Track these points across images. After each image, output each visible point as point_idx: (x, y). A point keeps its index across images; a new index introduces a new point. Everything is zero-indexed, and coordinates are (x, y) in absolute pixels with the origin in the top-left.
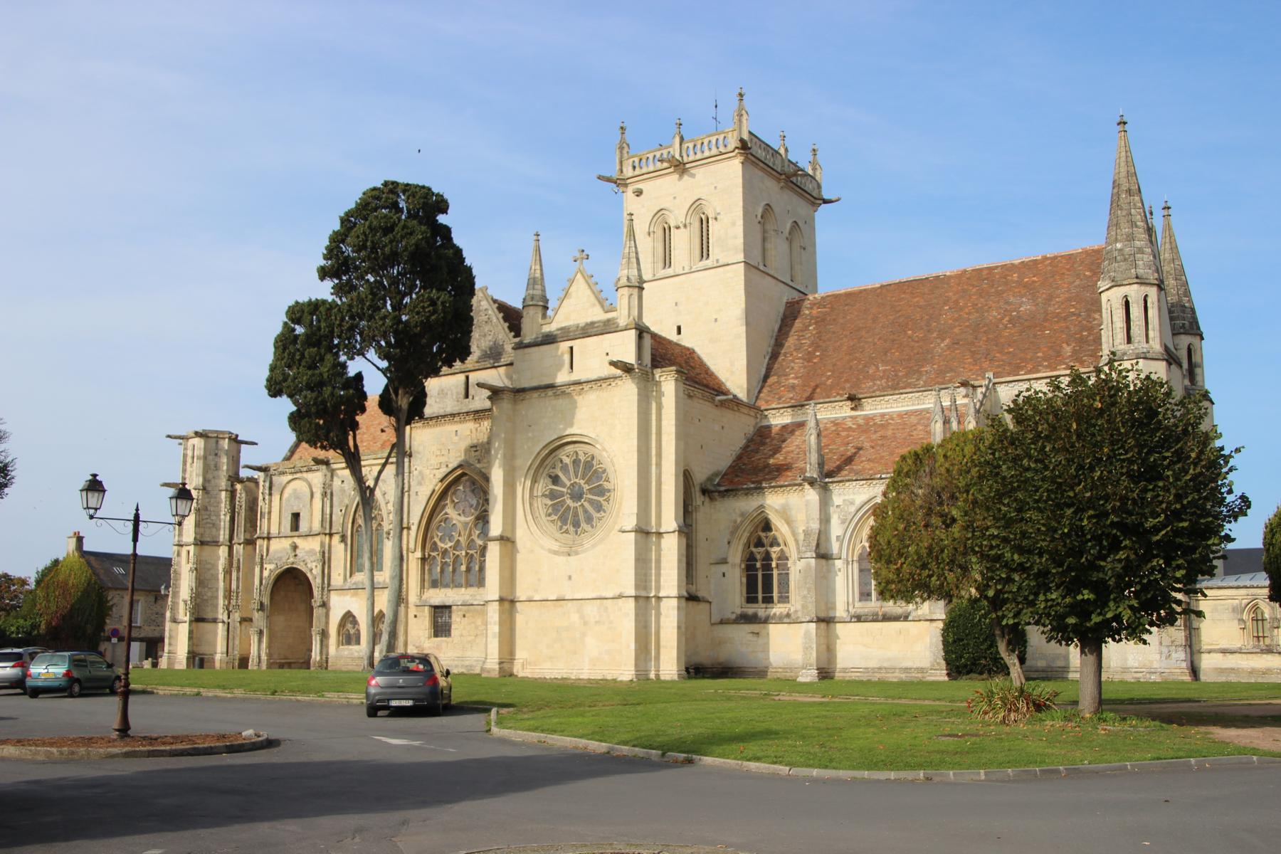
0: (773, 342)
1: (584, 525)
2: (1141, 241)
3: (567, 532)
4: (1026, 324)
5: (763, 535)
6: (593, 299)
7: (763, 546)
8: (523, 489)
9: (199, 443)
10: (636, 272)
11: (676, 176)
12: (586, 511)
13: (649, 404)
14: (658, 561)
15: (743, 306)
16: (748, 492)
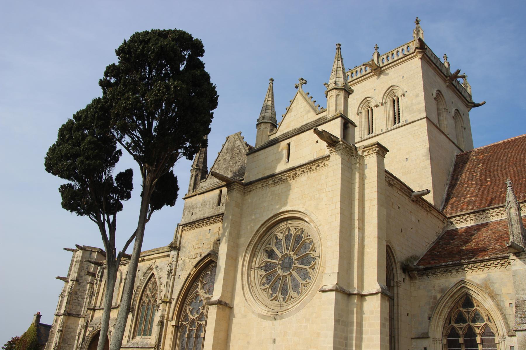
0: (450, 178)
1: (291, 292)
3: (276, 299)
7: (465, 321)
8: (242, 263)
9: (80, 253)
12: (294, 280)
13: (352, 174)
14: (360, 325)
16: (447, 270)
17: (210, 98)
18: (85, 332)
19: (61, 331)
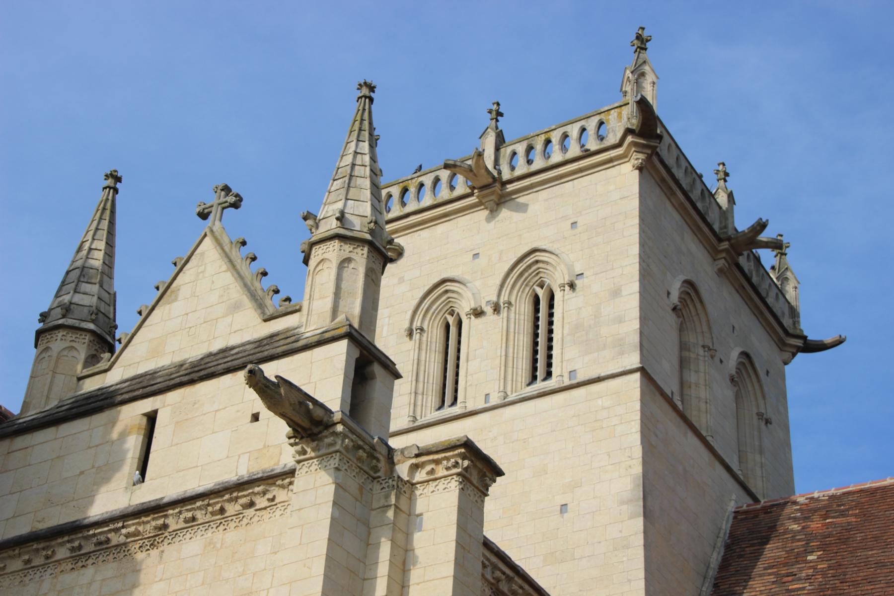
6: (236, 292)
10: (366, 209)
11: (482, 214)
13: (369, 546)
15: (638, 469)
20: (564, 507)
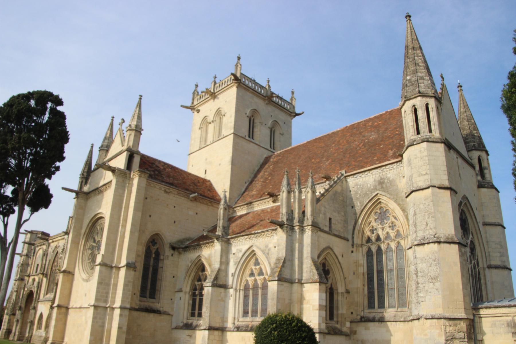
2: (423, 73)
4: (372, 144)
5: (201, 273)
11: (212, 100)
17: (64, 138)
18: (24, 292)
19: (17, 291)
20: (220, 164)
